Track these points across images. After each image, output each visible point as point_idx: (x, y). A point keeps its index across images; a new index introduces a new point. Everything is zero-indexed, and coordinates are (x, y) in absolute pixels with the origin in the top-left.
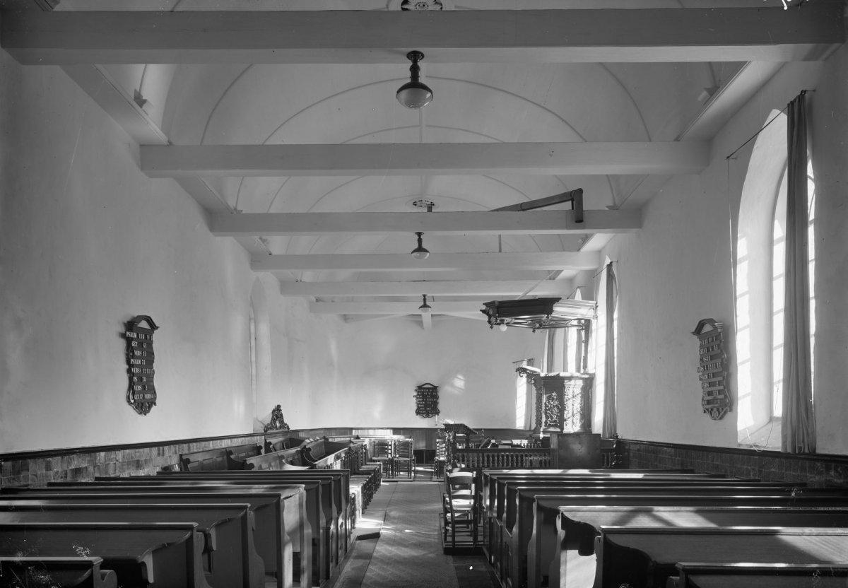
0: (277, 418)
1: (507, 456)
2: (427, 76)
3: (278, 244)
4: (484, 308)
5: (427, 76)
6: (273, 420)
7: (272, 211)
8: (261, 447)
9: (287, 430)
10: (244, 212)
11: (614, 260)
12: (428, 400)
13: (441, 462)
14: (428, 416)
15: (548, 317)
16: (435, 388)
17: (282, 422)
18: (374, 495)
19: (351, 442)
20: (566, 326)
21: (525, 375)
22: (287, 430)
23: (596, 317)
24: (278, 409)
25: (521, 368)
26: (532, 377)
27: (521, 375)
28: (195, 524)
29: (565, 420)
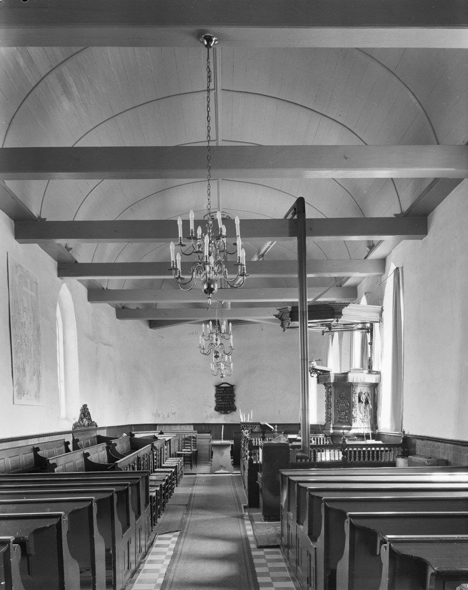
0: (85, 416)
1: (355, 452)
2: (222, 90)
3: (85, 251)
4: (277, 313)
5: (222, 90)
6: (81, 419)
7: (76, 219)
8: (68, 443)
9: (95, 427)
10: (47, 220)
11: (400, 266)
12: (225, 398)
13: (364, 451)
14: (226, 413)
15: (337, 321)
16: (232, 386)
17: (90, 419)
18: (175, 488)
19: (155, 438)
20: (352, 330)
21: (316, 375)
22: (95, 427)
23: (380, 321)
24: (85, 407)
25: (310, 534)
26: (323, 376)
27: (312, 375)
28: (93, 498)
29: (354, 418)
